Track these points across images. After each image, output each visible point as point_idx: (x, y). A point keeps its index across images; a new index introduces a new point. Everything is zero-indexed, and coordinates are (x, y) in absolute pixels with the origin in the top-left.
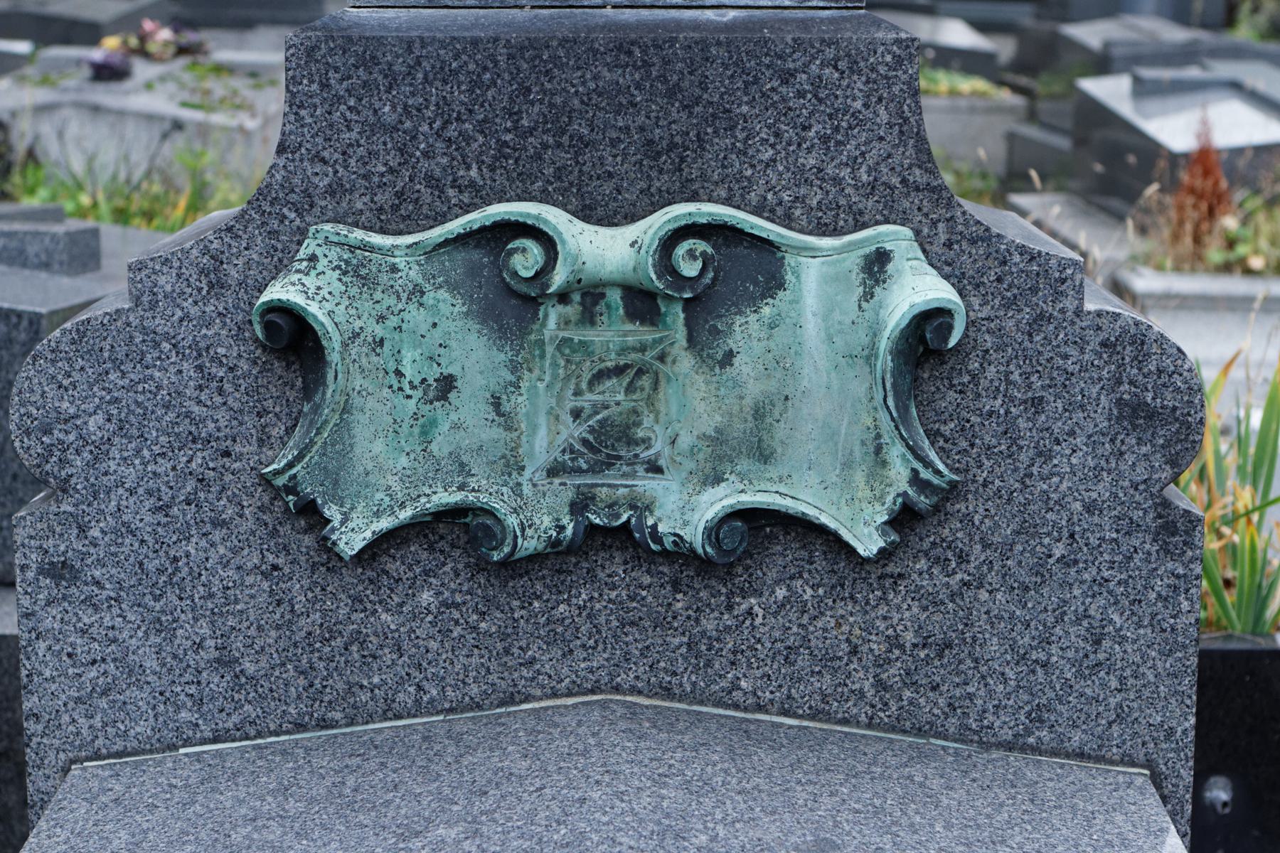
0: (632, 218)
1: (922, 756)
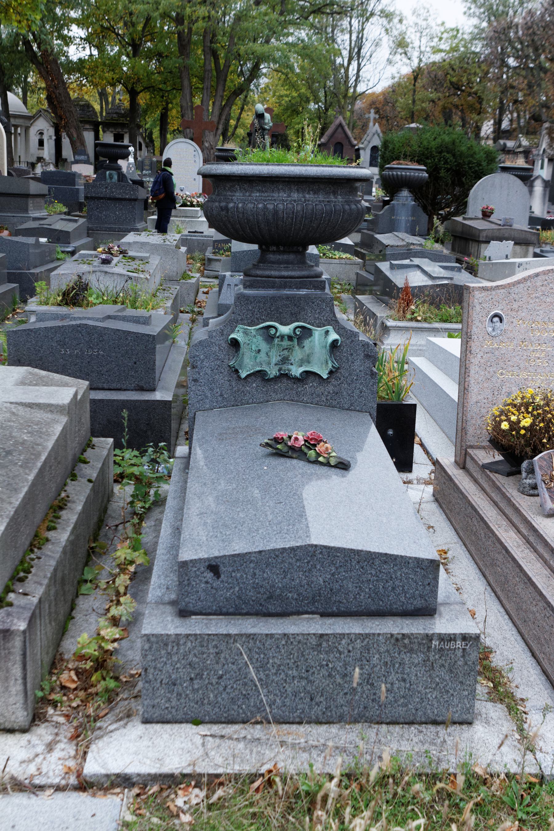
0: (288, 324)
1: (334, 410)
